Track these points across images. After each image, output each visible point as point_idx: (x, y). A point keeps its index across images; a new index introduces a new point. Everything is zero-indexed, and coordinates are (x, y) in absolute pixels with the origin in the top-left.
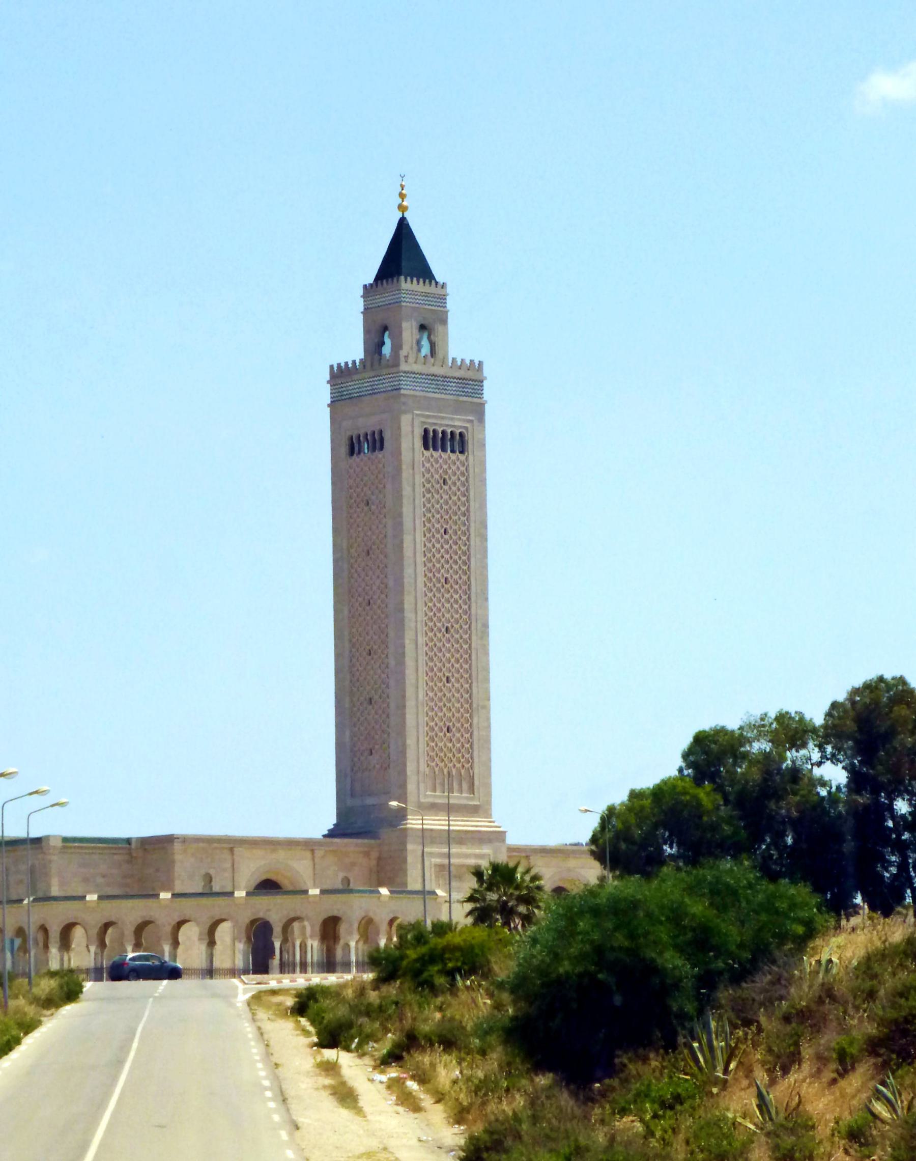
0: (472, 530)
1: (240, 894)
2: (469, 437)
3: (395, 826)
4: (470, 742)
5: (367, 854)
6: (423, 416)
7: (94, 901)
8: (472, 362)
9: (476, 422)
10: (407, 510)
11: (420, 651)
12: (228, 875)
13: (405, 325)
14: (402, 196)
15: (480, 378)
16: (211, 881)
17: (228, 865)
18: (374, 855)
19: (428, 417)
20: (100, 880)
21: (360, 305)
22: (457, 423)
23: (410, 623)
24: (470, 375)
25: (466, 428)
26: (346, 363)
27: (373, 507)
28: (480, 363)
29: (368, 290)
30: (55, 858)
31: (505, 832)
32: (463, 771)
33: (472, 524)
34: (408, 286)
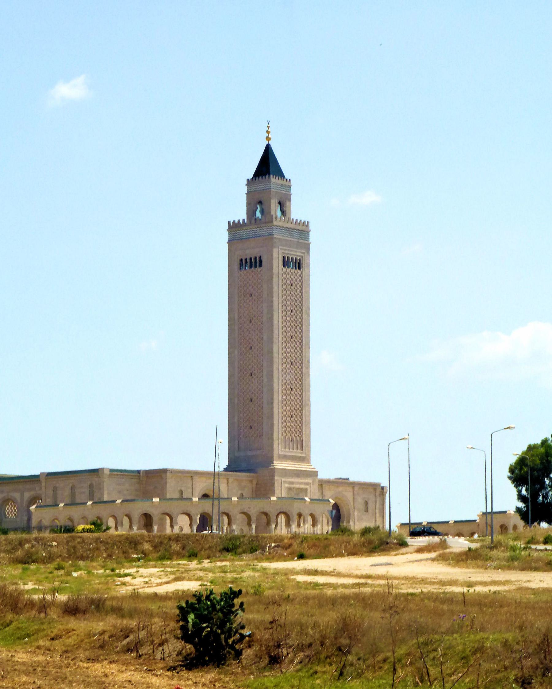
0: (304, 311)
1: (195, 499)
2: (303, 262)
3: (267, 467)
4: (301, 422)
5: (251, 481)
6: (283, 249)
7: (157, 502)
8: (296, 220)
9: (306, 254)
10: (275, 299)
11: (280, 375)
12: (190, 490)
13: (273, 201)
14: (268, 132)
15: (308, 230)
16: (182, 494)
17: (190, 485)
18: (255, 482)
19: (285, 250)
20: (125, 492)
21: (245, 190)
22: (298, 254)
23: (276, 360)
24: (304, 228)
25: (302, 257)
26: (239, 221)
27: (254, 298)
28: (308, 222)
29: (249, 183)
30: (105, 480)
31: (317, 472)
32: (298, 438)
33: (304, 308)
34: (274, 180)
